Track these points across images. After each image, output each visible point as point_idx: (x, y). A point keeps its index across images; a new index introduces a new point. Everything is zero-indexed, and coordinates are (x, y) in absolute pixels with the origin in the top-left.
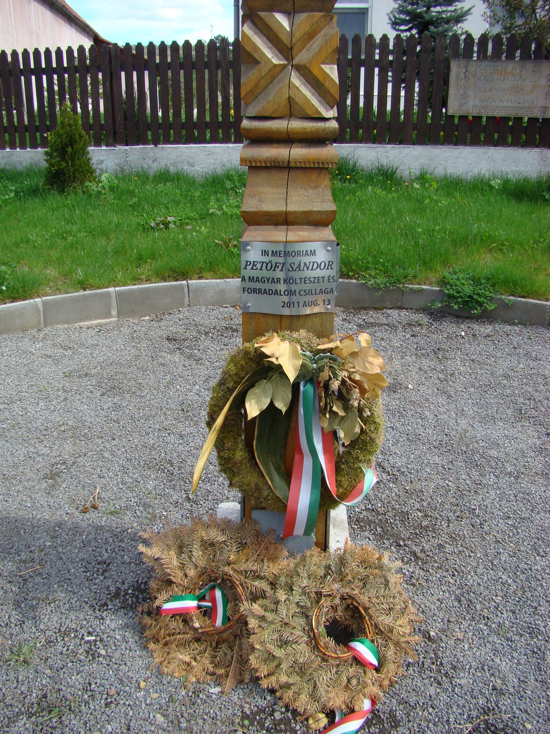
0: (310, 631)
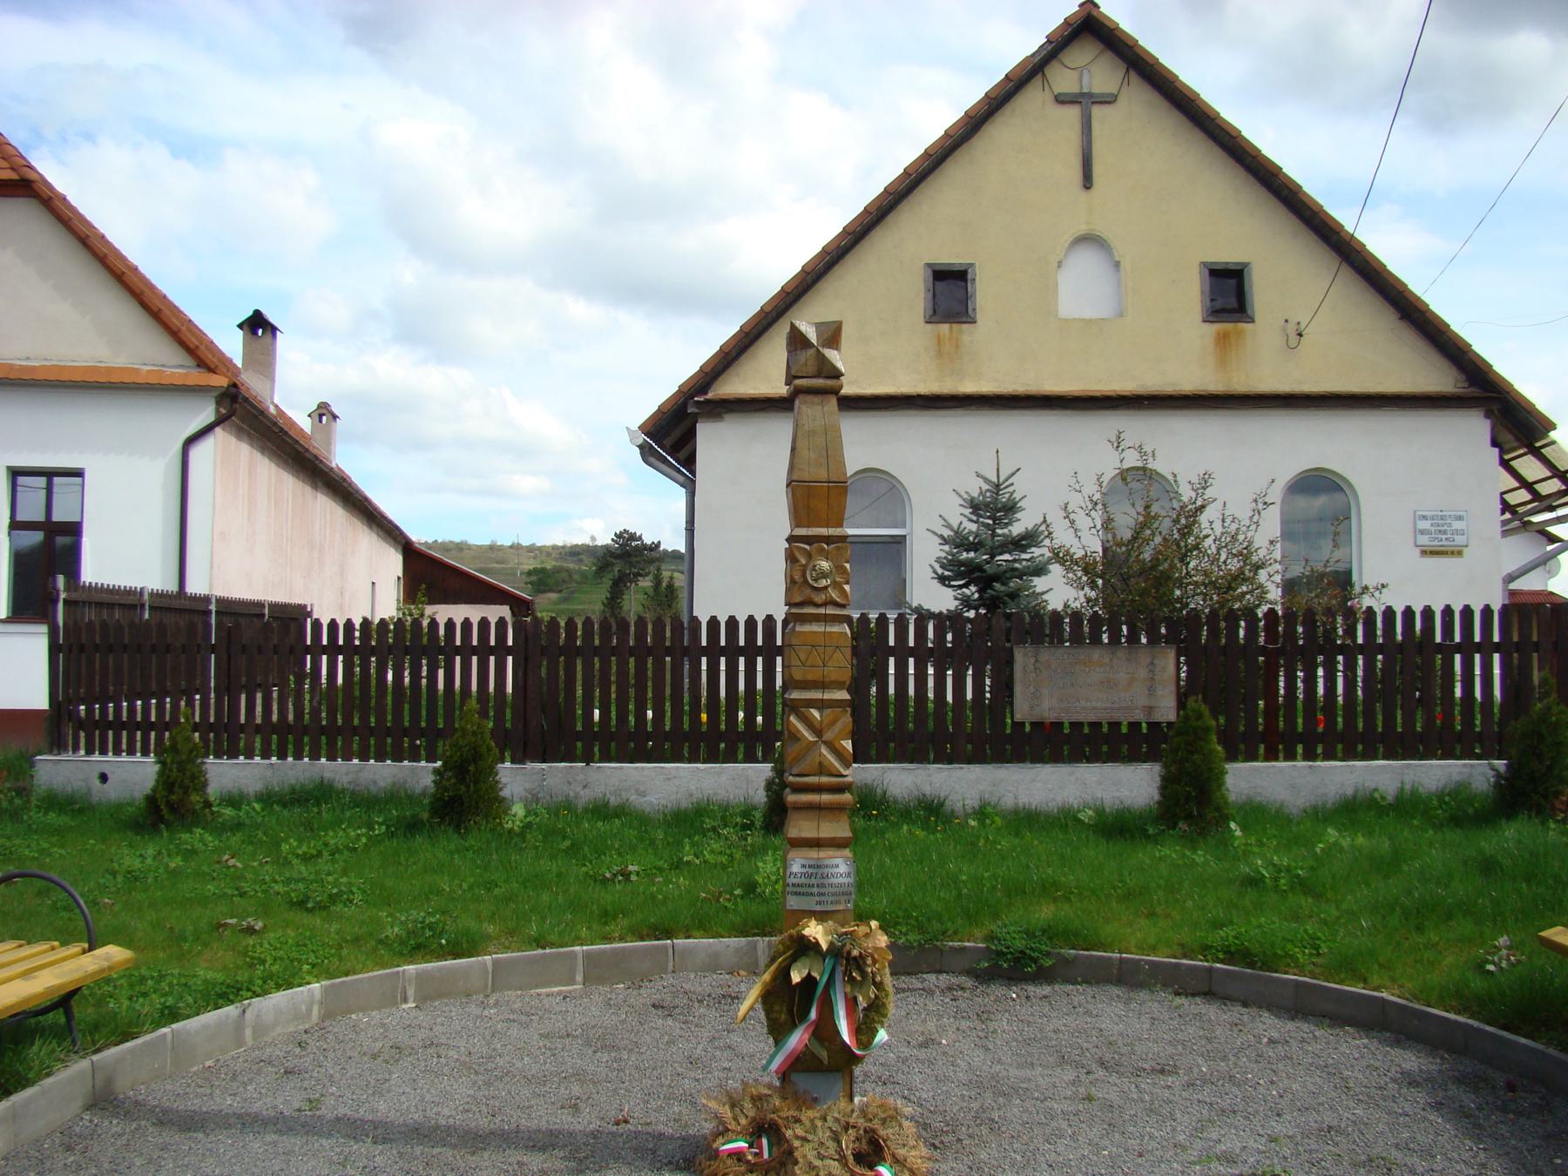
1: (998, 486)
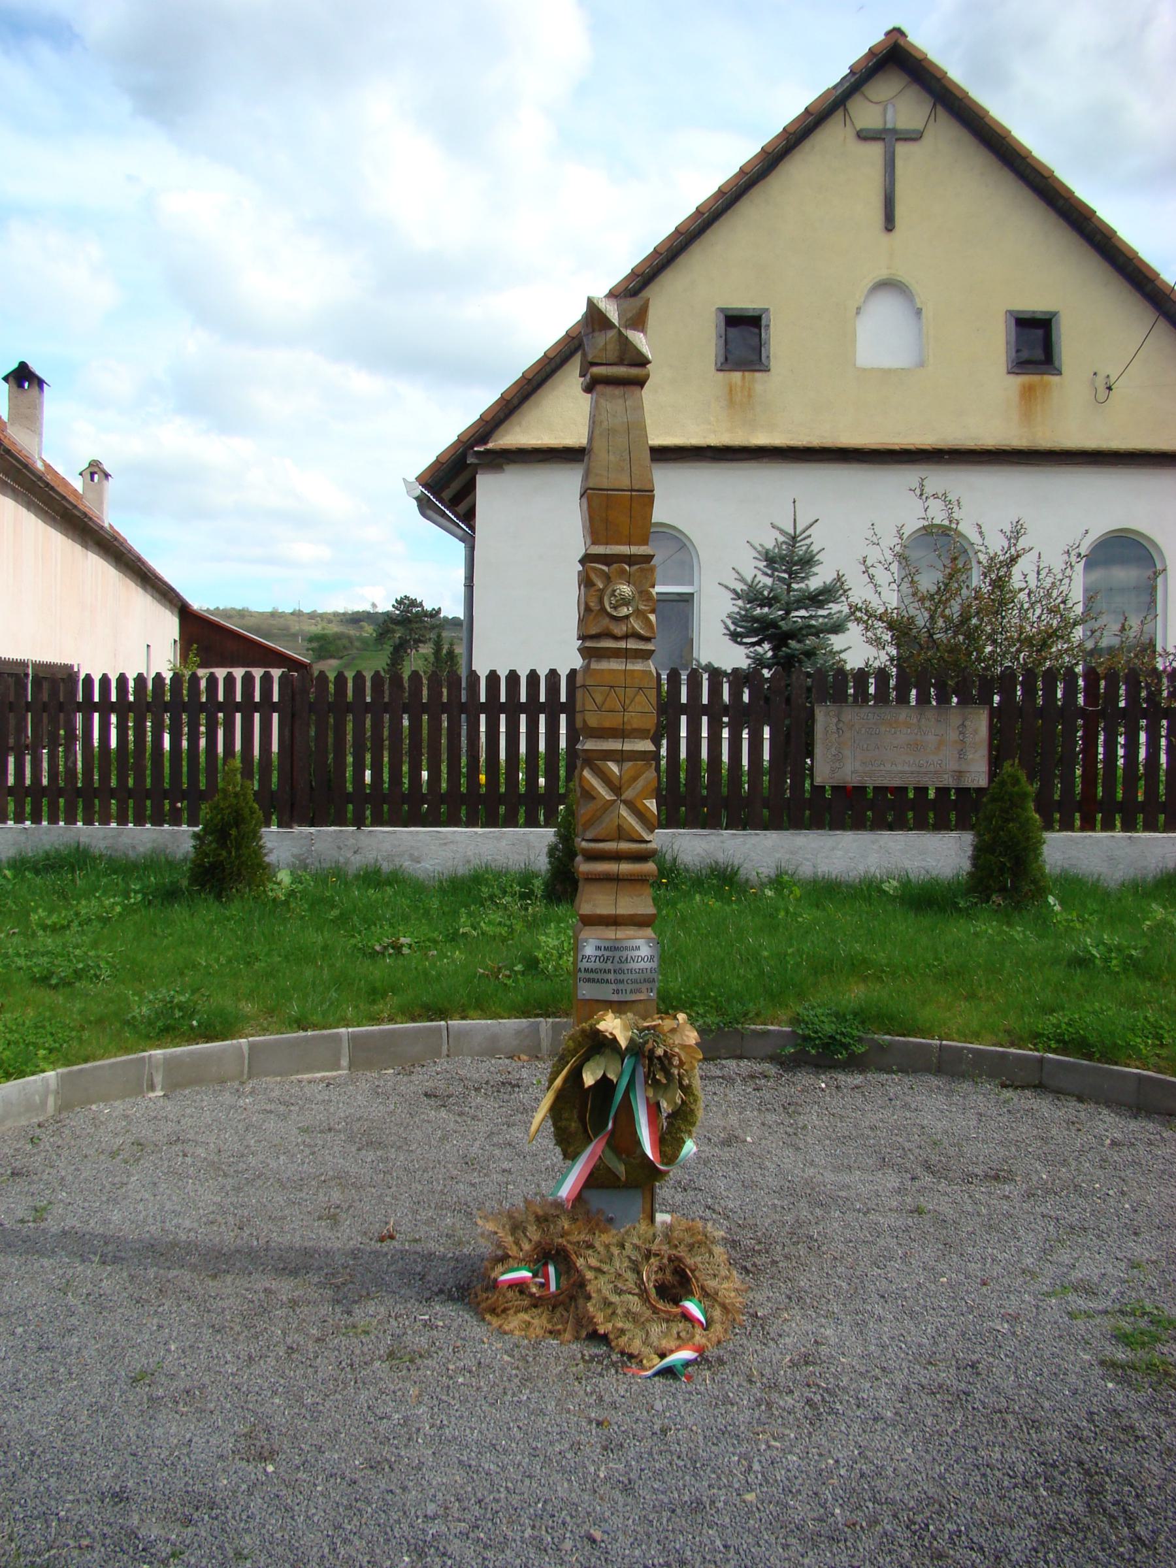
0: (640, 1283)
1: (794, 538)
